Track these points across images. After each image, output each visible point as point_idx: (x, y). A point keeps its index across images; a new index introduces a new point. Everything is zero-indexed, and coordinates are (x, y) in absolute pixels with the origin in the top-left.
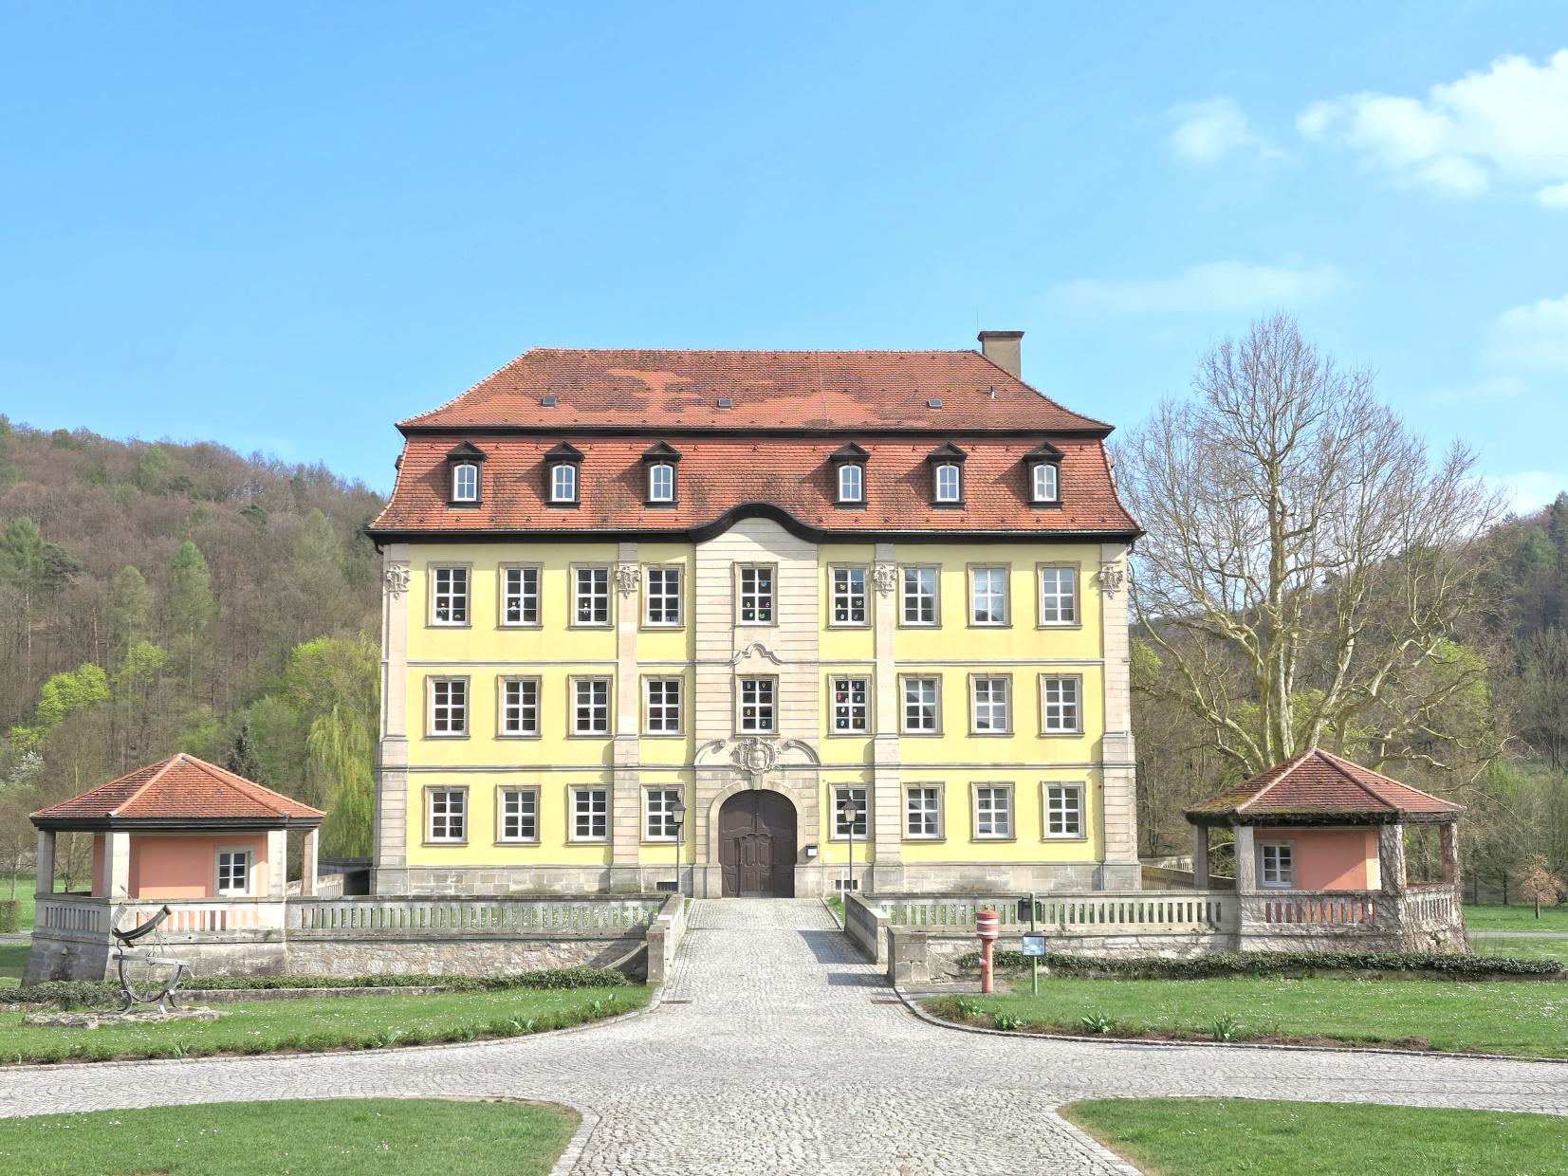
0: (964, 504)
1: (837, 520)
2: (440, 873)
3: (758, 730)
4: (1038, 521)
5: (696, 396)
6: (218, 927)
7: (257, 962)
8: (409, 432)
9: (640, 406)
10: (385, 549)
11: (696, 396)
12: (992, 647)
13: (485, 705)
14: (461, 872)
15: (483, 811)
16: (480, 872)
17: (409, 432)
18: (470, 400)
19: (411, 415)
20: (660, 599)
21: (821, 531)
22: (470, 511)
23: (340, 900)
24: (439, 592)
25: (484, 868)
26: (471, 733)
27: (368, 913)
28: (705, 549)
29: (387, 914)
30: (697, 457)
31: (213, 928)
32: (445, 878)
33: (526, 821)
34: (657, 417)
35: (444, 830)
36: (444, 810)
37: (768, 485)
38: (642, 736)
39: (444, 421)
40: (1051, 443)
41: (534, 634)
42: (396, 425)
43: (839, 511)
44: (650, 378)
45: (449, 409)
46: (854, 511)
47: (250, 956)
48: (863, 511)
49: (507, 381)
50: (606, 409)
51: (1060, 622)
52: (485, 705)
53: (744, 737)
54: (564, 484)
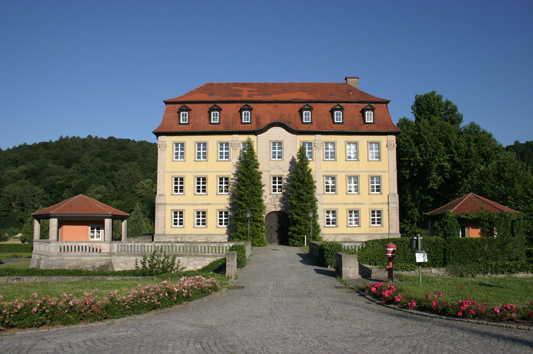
0: (312, 123)
1: (303, 128)
2: (176, 236)
3: (277, 193)
4: (367, 128)
5: (257, 93)
6: (133, 251)
7: (100, 263)
8: (167, 103)
9: (240, 96)
10: (159, 137)
11: (257, 93)
12: (353, 168)
13: (190, 185)
14: (182, 236)
15: (190, 218)
16: (188, 236)
17: (167, 103)
18: (187, 95)
19: (165, 100)
20: (328, 152)
21: (298, 131)
22: (185, 126)
23: (225, 242)
24: (198, 150)
25: (189, 235)
26: (208, 193)
27: (140, 247)
28: (262, 136)
29: (146, 248)
30: (258, 108)
31: (131, 251)
32: (177, 238)
33: (203, 220)
34: (245, 97)
35: (202, 221)
36: (375, 216)
37: (281, 117)
38: (324, 194)
39: (181, 100)
40: (249, 104)
41: (206, 162)
42: (163, 101)
43: (303, 125)
44: (242, 89)
45: (181, 97)
46: (308, 125)
47: (99, 261)
48: (311, 125)
49: (199, 90)
50: (230, 97)
51: (374, 159)
52: (190, 185)
53: (273, 194)
54: (184, 118)
